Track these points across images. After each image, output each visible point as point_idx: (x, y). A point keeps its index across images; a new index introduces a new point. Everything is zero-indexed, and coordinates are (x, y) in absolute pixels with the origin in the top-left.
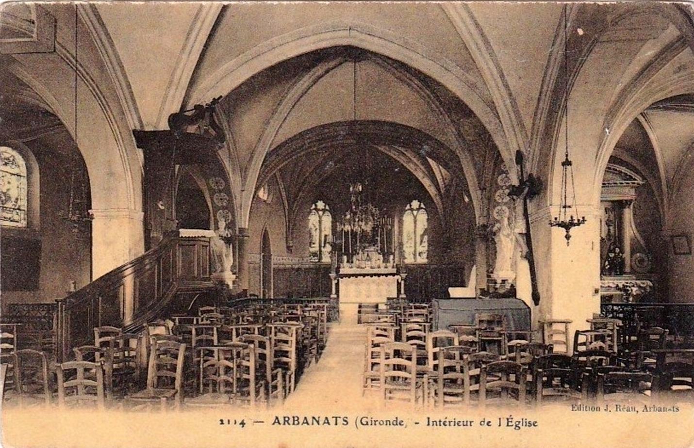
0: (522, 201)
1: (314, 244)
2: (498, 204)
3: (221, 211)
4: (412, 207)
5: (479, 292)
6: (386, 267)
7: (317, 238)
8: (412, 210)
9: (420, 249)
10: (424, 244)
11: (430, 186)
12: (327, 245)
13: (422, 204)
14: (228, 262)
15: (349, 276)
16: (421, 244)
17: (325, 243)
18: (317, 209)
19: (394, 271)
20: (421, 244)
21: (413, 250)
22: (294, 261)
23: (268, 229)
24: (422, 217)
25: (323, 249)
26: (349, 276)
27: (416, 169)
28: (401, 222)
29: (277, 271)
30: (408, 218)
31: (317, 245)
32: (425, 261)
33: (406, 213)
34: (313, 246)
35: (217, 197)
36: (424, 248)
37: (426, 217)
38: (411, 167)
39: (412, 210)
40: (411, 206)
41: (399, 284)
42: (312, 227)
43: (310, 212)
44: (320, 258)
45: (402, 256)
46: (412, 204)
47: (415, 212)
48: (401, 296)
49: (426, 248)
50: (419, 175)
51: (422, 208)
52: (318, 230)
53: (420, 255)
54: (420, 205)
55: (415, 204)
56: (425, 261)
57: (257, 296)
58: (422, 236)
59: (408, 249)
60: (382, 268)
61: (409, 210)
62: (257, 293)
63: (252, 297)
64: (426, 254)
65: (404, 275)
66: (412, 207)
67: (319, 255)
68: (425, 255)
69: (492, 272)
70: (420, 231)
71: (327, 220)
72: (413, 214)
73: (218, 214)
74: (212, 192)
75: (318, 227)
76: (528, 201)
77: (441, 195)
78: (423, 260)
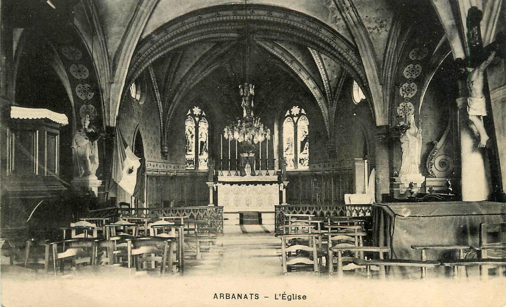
0: (481, 73)
1: (190, 151)
2: (403, 99)
3: (80, 85)
4: (292, 113)
5: (380, 198)
6: (268, 175)
7: (194, 144)
8: (292, 116)
9: (300, 156)
10: (305, 151)
11: (315, 88)
12: (205, 153)
13: (303, 110)
14: (93, 167)
15: (224, 183)
16: (302, 151)
17: (201, 151)
18: (193, 116)
19: (275, 178)
20: (302, 151)
21: (293, 157)
22: (169, 169)
23: (141, 131)
24: (304, 124)
25: (199, 157)
26: (224, 183)
27: (300, 70)
28: (280, 129)
29: (150, 177)
30: (288, 125)
31: (193, 152)
32: (306, 168)
33: (286, 120)
34: (189, 153)
35: (80, 89)
36: (304, 155)
37: (308, 124)
38: (295, 67)
39: (292, 116)
40: (290, 112)
41: (281, 192)
42: (188, 133)
43: (186, 118)
44: (197, 165)
45: (282, 162)
46: (292, 110)
47: (295, 119)
48: (282, 204)
49: (308, 155)
50: (303, 76)
51: (303, 114)
52: (194, 137)
53: (300, 162)
54: (300, 111)
55: (295, 110)
56: (306, 168)
57: (128, 205)
58: (303, 144)
59: (289, 156)
60: (264, 176)
61: (288, 116)
62: (128, 202)
63: (123, 207)
64: (307, 161)
65: (286, 183)
66: (292, 113)
67: (196, 162)
68: (306, 162)
69: (397, 176)
70: (301, 138)
71: (204, 127)
72: (294, 121)
73: (77, 89)
74: (74, 83)
75: (194, 133)
76: (488, 73)
77: (326, 98)
78: (304, 167)
